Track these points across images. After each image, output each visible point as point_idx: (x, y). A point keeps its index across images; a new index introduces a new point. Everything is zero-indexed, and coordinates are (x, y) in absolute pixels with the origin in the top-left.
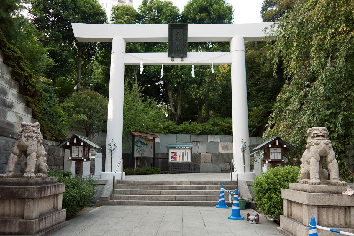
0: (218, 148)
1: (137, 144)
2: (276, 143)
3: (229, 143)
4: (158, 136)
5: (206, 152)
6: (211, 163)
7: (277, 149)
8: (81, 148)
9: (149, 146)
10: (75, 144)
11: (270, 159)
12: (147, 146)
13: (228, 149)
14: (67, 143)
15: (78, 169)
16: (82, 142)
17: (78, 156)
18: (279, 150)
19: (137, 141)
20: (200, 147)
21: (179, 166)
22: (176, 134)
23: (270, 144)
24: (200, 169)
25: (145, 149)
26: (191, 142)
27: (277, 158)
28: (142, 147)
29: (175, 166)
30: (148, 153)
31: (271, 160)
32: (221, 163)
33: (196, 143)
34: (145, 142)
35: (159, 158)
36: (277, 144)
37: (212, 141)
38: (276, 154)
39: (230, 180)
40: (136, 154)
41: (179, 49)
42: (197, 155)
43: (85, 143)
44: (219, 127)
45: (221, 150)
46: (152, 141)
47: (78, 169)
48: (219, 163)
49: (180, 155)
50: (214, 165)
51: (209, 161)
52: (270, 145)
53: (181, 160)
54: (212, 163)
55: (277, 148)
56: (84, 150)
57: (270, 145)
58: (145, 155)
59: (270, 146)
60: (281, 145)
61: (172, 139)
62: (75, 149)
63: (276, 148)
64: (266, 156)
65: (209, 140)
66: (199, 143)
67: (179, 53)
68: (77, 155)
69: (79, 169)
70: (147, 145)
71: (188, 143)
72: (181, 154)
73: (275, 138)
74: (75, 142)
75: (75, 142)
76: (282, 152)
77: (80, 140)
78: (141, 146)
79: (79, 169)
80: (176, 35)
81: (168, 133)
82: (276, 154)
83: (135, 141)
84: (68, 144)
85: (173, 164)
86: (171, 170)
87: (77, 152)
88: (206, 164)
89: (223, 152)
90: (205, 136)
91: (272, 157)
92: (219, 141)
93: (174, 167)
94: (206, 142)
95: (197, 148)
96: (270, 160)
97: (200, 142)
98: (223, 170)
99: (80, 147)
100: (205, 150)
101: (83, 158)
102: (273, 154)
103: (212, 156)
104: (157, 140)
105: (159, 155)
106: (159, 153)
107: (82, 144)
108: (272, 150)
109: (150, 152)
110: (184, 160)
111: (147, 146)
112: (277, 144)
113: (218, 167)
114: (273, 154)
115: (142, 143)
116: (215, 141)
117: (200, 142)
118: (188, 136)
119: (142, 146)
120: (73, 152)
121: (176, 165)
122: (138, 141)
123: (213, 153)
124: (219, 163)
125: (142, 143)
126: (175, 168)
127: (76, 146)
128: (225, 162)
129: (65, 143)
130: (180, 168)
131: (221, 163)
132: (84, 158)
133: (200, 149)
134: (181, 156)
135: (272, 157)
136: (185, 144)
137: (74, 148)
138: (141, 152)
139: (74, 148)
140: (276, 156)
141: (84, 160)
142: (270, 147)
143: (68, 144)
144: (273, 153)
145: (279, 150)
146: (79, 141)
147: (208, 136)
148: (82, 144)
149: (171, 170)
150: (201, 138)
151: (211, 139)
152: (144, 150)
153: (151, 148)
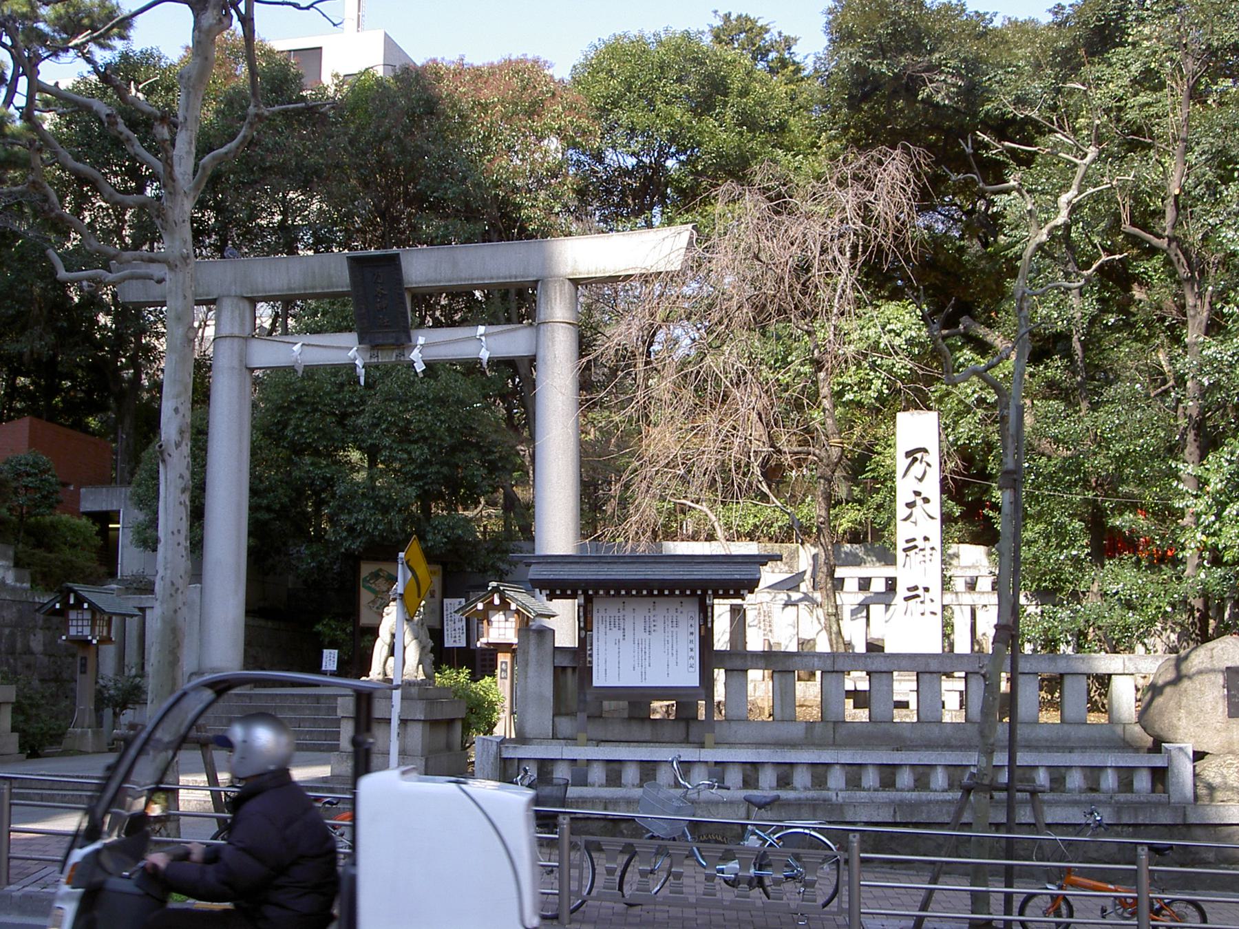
8: (88, 615)
10: (73, 607)
56: (93, 619)
74: (72, 602)
75: (72, 602)
84: (58, 606)
107: (86, 606)
137: (73, 615)
139: (73, 615)
148: (86, 606)
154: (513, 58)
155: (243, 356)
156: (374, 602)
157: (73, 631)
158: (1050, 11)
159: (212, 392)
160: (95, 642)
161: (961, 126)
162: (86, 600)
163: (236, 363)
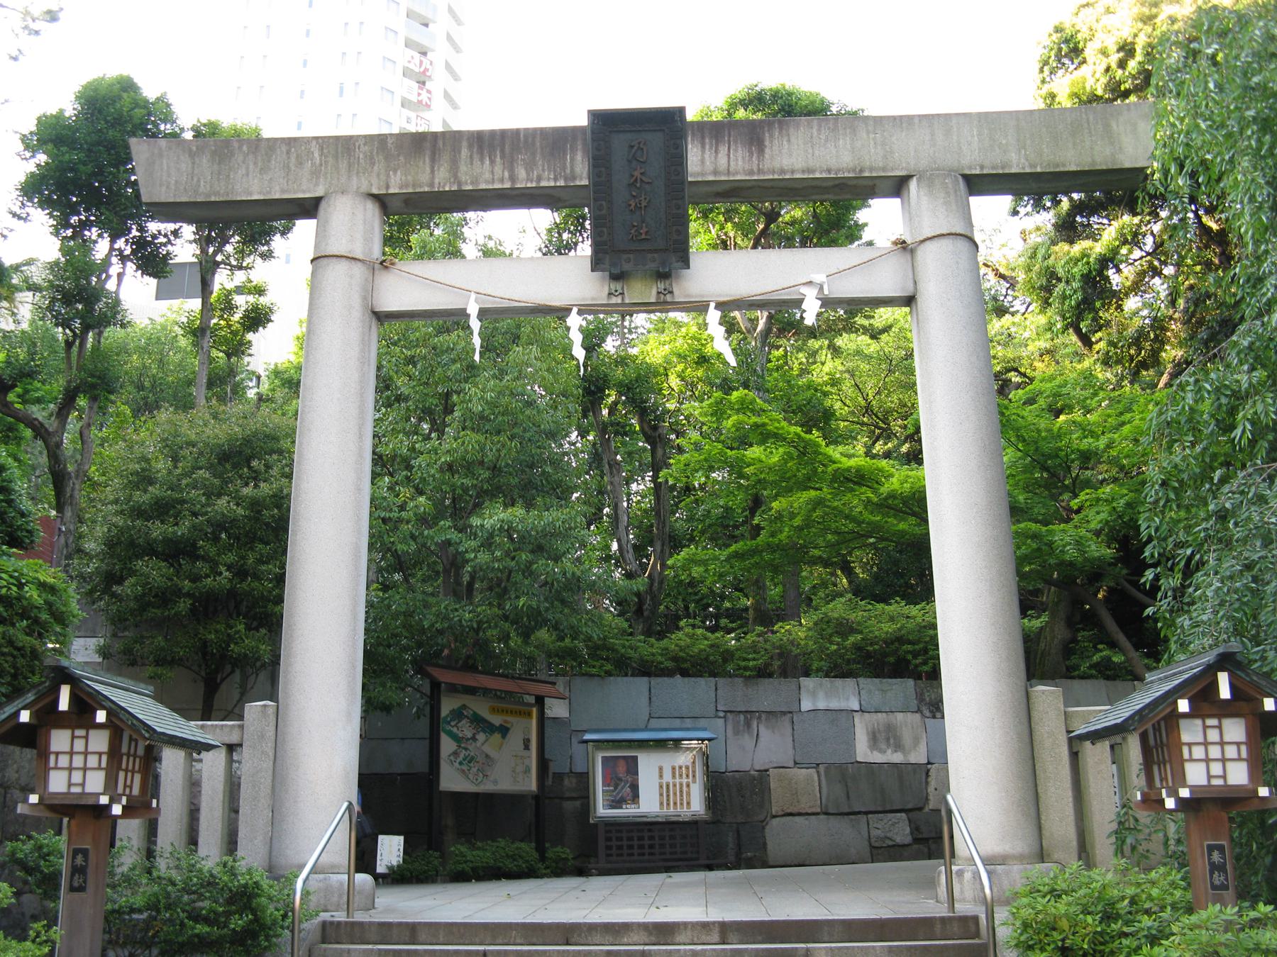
0: (850, 743)
1: (455, 730)
2: (1214, 685)
3: (900, 716)
4: (561, 690)
5: (791, 764)
6: (822, 817)
7: (1220, 727)
8: (100, 741)
9: (515, 739)
10: (62, 721)
11: (1184, 785)
12: (504, 736)
13: (898, 747)
14: (17, 714)
15: (79, 860)
16: (103, 708)
17: (83, 785)
18: (1235, 730)
19: (452, 712)
20: (761, 739)
21: (646, 834)
22: (646, 679)
23: (1181, 697)
24: (765, 844)
25: (492, 753)
26: (722, 714)
27: (1224, 777)
28: (479, 744)
29: (646, 834)
30: (509, 770)
31: (1193, 789)
32: (867, 813)
33: (742, 717)
34: (496, 720)
35: (567, 795)
36: (1225, 692)
37: (821, 705)
38: (1215, 752)
39: (941, 911)
40: (452, 780)
41: (646, 233)
42: (754, 778)
43: (115, 712)
44: (852, 639)
45: (863, 751)
46: (530, 715)
47: (79, 860)
48: (859, 813)
49: (671, 781)
50: (834, 822)
51: (809, 802)
52: (1180, 701)
53: (675, 804)
54: (826, 814)
55: (1220, 716)
56: (114, 753)
57: (1180, 701)
58: (495, 782)
59: (1183, 706)
60: (1243, 703)
61: (630, 695)
62: (68, 749)
63: (1212, 722)
64: (1155, 768)
65: (806, 705)
66: (759, 718)
67: (650, 251)
68: (73, 781)
69: (86, 860)
70: (504, 731)
71: (702, 722)
72: (674, 777)
73: (1209, 658)
74: (64, 705)
75: (64, 705)
76: (1249, 743)
77: (89, 694)
78: (474, 738)
79: (86, 860)
80: (629, 161)
81: (609, 673)
82: (1215, 752)
83: (445, 711)
84: (25, 716)
85: (614, 826)
86: (608, 855)
87: (74, 765)
88: (797, 819)
89: (877, 757)
90: (786, 685)
91: (1196, 775)
92: (856, 707)
93: (620, 839)
94: (789, 713)
95: (748, 741)
96: (1184, 793)
97: (764, 716)
98: (876, 845)
99: (93, 733)
100: (791, 752)
101: (104, 800)
102: (1198, 752)
103: (823, 778)
104: (557, 709)
105: (566, 782)
106: (567, 770)
107: (101, 716)
108: (1190, 732)
109: (520, 769)
110: (688, 803)
111: (504, 736)
112: (1225, 692)
113: (848, 833)
114: (1198, 752)
115: (478, 721)
116: (834, 705)
117: (764, 716)
118: (703, 687)
119: (481, 737)
120: (52, 764)
121: (620, 831)
122: (458, 714)
123: (829, 766)
124: (859, 813)
125: (478, 721)
126: (647, 842)
127: (73, 727)
128: (888, 808)
129: (9, 710)
130: (662, 846)
131: (867, 813)
132: (112, 800)
133: (765, 750)
134: (675, 785)
135: (1196, 775)
136: (688, 723)
137: (59, 740)
138: (475, 770)
139: (59, 740)
140: (1216, 769)
141: (108, 808)
142: (1185, 715)
143: (25, 716)
144: (1218, 748)
145: (1235, 730)
146: (84, 705)
147: (804, 681)
148: (101, 716)
149: (608, 855)
150: (768, 694)
151: (818, 696)
152: (487, 756)
153: (527, 747)
154: (267, 134)
155: (369, 292)
156: (455, 754)
157: (57, 783)
158: (866, 225)
159: (835, 249)
160: (117, 810)
161: (283, 385)
162: (102, 701)
163: (356, 302)
